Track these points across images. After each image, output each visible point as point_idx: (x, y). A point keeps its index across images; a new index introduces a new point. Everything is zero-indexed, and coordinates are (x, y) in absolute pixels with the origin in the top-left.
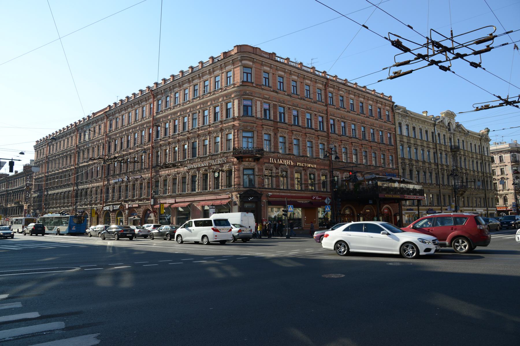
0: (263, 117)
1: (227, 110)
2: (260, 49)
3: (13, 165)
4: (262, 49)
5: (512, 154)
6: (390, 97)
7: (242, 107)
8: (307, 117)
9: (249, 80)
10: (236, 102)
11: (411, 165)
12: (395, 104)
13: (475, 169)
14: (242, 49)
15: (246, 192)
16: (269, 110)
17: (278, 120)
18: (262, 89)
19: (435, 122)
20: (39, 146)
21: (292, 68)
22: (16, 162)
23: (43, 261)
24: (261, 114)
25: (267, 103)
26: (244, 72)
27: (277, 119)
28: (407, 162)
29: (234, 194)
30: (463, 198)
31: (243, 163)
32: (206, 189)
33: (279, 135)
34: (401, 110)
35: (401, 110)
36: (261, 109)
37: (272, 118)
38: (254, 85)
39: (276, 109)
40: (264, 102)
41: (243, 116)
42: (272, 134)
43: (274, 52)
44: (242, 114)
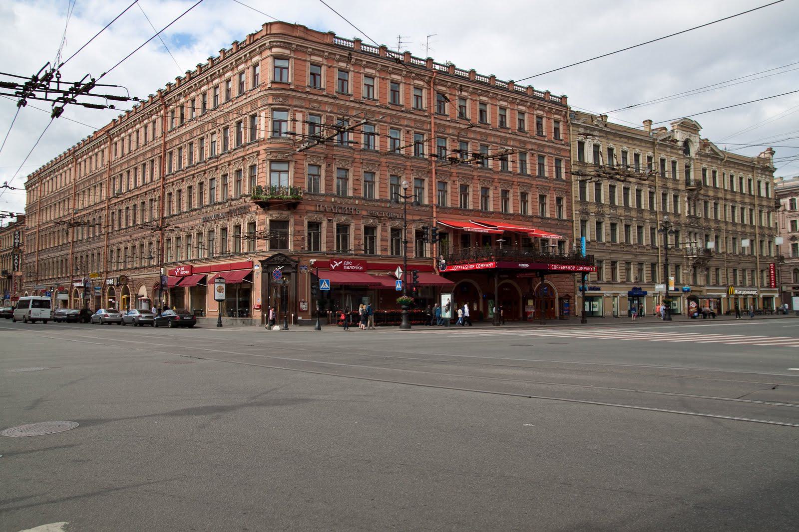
4: (309, 28)
6: (564, 98)
9: (284, 80)
20: (34, 182)
26: (275, 67)
33: (334, 168)
35: (582, 120)
38: (292, 87)
41: (272, 138)
42: (324, 166)
43: (332, 30)
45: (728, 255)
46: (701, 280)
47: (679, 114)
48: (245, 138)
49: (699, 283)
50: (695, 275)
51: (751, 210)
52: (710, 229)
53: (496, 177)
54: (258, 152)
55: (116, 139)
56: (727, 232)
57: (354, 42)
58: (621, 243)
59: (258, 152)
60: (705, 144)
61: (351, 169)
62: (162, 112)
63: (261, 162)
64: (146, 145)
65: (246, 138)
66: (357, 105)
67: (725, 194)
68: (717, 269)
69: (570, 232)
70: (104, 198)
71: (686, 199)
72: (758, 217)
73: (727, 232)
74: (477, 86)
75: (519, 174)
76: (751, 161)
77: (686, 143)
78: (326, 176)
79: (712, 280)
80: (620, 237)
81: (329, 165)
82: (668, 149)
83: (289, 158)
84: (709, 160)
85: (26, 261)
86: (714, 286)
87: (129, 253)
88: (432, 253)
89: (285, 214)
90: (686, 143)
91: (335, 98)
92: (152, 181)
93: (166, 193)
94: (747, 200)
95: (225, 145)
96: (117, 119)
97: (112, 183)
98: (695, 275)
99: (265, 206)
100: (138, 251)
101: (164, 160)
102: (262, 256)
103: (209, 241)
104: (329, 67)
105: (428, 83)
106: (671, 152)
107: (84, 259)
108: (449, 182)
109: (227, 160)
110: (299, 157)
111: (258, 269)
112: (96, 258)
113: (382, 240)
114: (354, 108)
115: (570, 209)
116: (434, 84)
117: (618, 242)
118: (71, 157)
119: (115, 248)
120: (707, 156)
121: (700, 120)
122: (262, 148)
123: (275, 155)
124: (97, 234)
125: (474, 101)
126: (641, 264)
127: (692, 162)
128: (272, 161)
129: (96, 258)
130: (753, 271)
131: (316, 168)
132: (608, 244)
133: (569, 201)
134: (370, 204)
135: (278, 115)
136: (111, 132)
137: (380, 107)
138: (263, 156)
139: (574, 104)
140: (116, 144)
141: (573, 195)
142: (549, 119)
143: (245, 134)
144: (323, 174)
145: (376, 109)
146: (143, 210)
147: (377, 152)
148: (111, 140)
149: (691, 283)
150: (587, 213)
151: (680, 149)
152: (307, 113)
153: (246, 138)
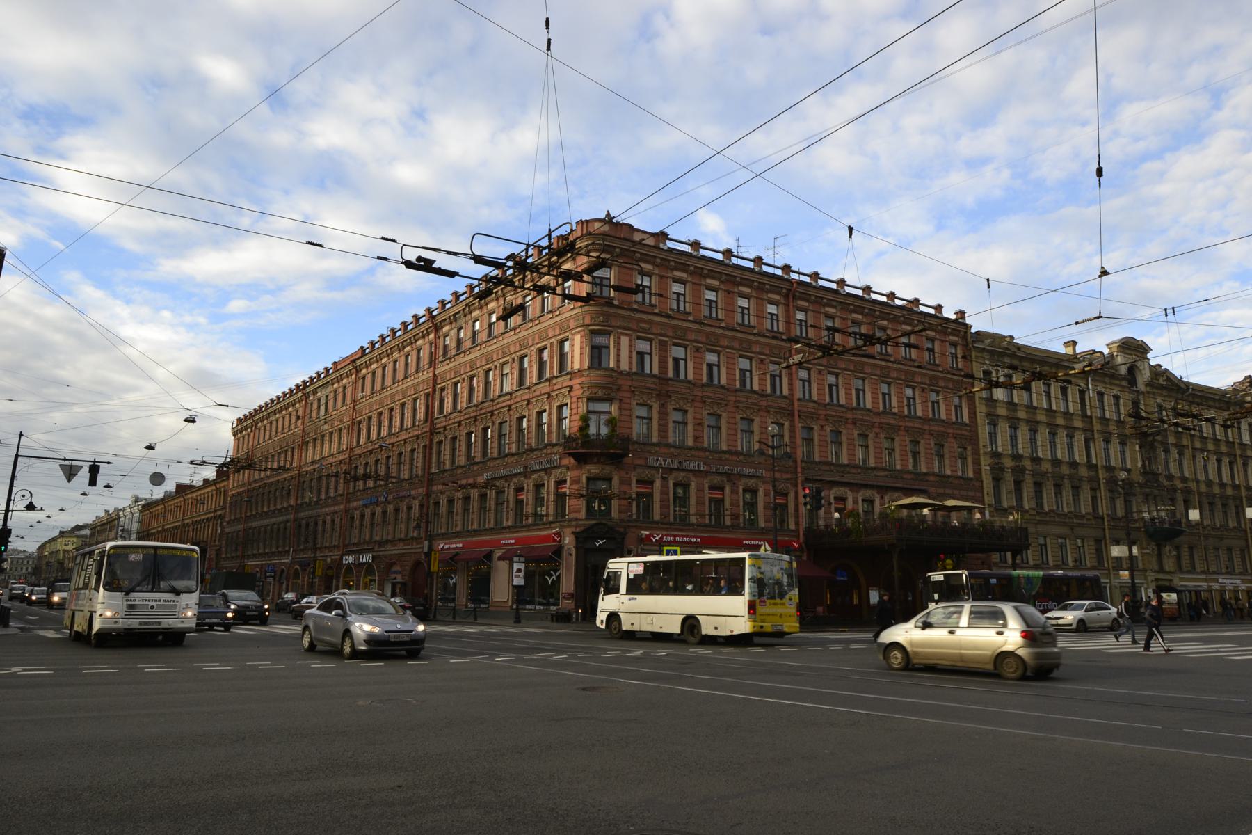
0: (634, 370)
1: (562, 356)
2: (630, 226)
3: (98, 471)
5: (594, 469)
7: (634, 354)
8: (741, 366)
10: (577, 338)
11: (1019, 471)
12: (973, 330)
13: (1213, 476)
14: (614, 243)
15: (589, 529)
16: (718, 366)
17: (671, 374)
18: (854, 355)
19: (1100, 369)
21: (704, 262)
22: (103, 468)
23: (967, 500)
24: (630, 363)
25: (746, 357)
27: (666, 373)
28: (1008, 463)
29: (568, 531)
30: (1178, 548)
31: (588, 467)
32: (521, 521)
33: (670, 407)
34: (987, 342)
35: (987, 342)
36: (630, 352)
37: (656, 371)
39: (666, 351)
40: (639, 338)
42: (656, 406)
44: (586, 365)
45: (1204, 528)
46: (1169, 564)
47: (1118, 334)
48: (552, 368)
49: (1167, 568)
50: (1160, 556)
51: (1231, 463)
52: (1175, 490)
53: (877, 420)
54: (571, 387)
55: (364, 371)
56: (1200, 494)
57: (754, 261)
58: (1051, 511)
59: (571, 387)
60: (1158, 372)
61: (691, 411)
62: (432, 336)
63: (574, 399)
64: (406, 378)
65: (551, 369)
66: (697, 326)
67: (1192, 442)
68: (1191, 548)
69: (978, 494)
70: (344, 447)
71: (1137, 448)
72: (1242, 474)
73: (1200, 494)
74: (765, 280)
75: (737, 390)
76: (1222, 393)
77: (1132, 369)
78: (660, 419)
79: (1186, 563)
80: (1048, 503)
81: (662, 406)
82: (1107, 380)
83: (613, 395)
84: (1164, 393)
85: (227, 530)
86: (1189, 572)
87: (378, 519)
88: (797, 524)
89: (608, 469)
90: (1132, 369)
91: (668, 316)
92: (414, 425)
93: (436, 440)
94: (1224, 449)
95: (521, 381)
96: (366, 345)
97: (355, 427)
98: (1160, 556)
99: (581, 459)
100: (391, 517)
101: (433, 398)
102: (576, 526)
103: (497, 504)
104: (661, 277)
105: (786, 296)
106: (1111, 384)
107: (311, 528)
108: (871, 435)
109: (526, 397)
110: (625, 394)
111: (568, 540)
112: (328, 526)
113: (697, 503)
114: (659, 323)
115: (977, 463)
116: (794, 297)
117: (1046, 509)
118: (300, 394)
119: (357, 514)
120: (1161, 387)
121: (668, 231)
122: (576, 382)
123: (594, 391)
124: (323, 497)
125: (729, 292)
126: (1229, 550)
127: (1141, 397)
128: (590, 399)
129: (328, 526)
130: (1242, 551)
131: (645, 409)
132: (1033, 512)
133: (976, 452)
134: (716, 456)
135: (600, 340)
136: (358, 363)
137: (759, 335)
138: (577, 392)
139: (977, 323)
140: (364, 378)
141: (981, 444)
142: (942, 341)
143: (552, 363)
144: (655, 416)
145: (721, 331)
146: (399, 463)
147: (723, 387)
148: (357, 372)
149: (1156, 567)
150: (1002, 469)
151: (1124, 379)
152: (634, 336)
153: (551, 369)
